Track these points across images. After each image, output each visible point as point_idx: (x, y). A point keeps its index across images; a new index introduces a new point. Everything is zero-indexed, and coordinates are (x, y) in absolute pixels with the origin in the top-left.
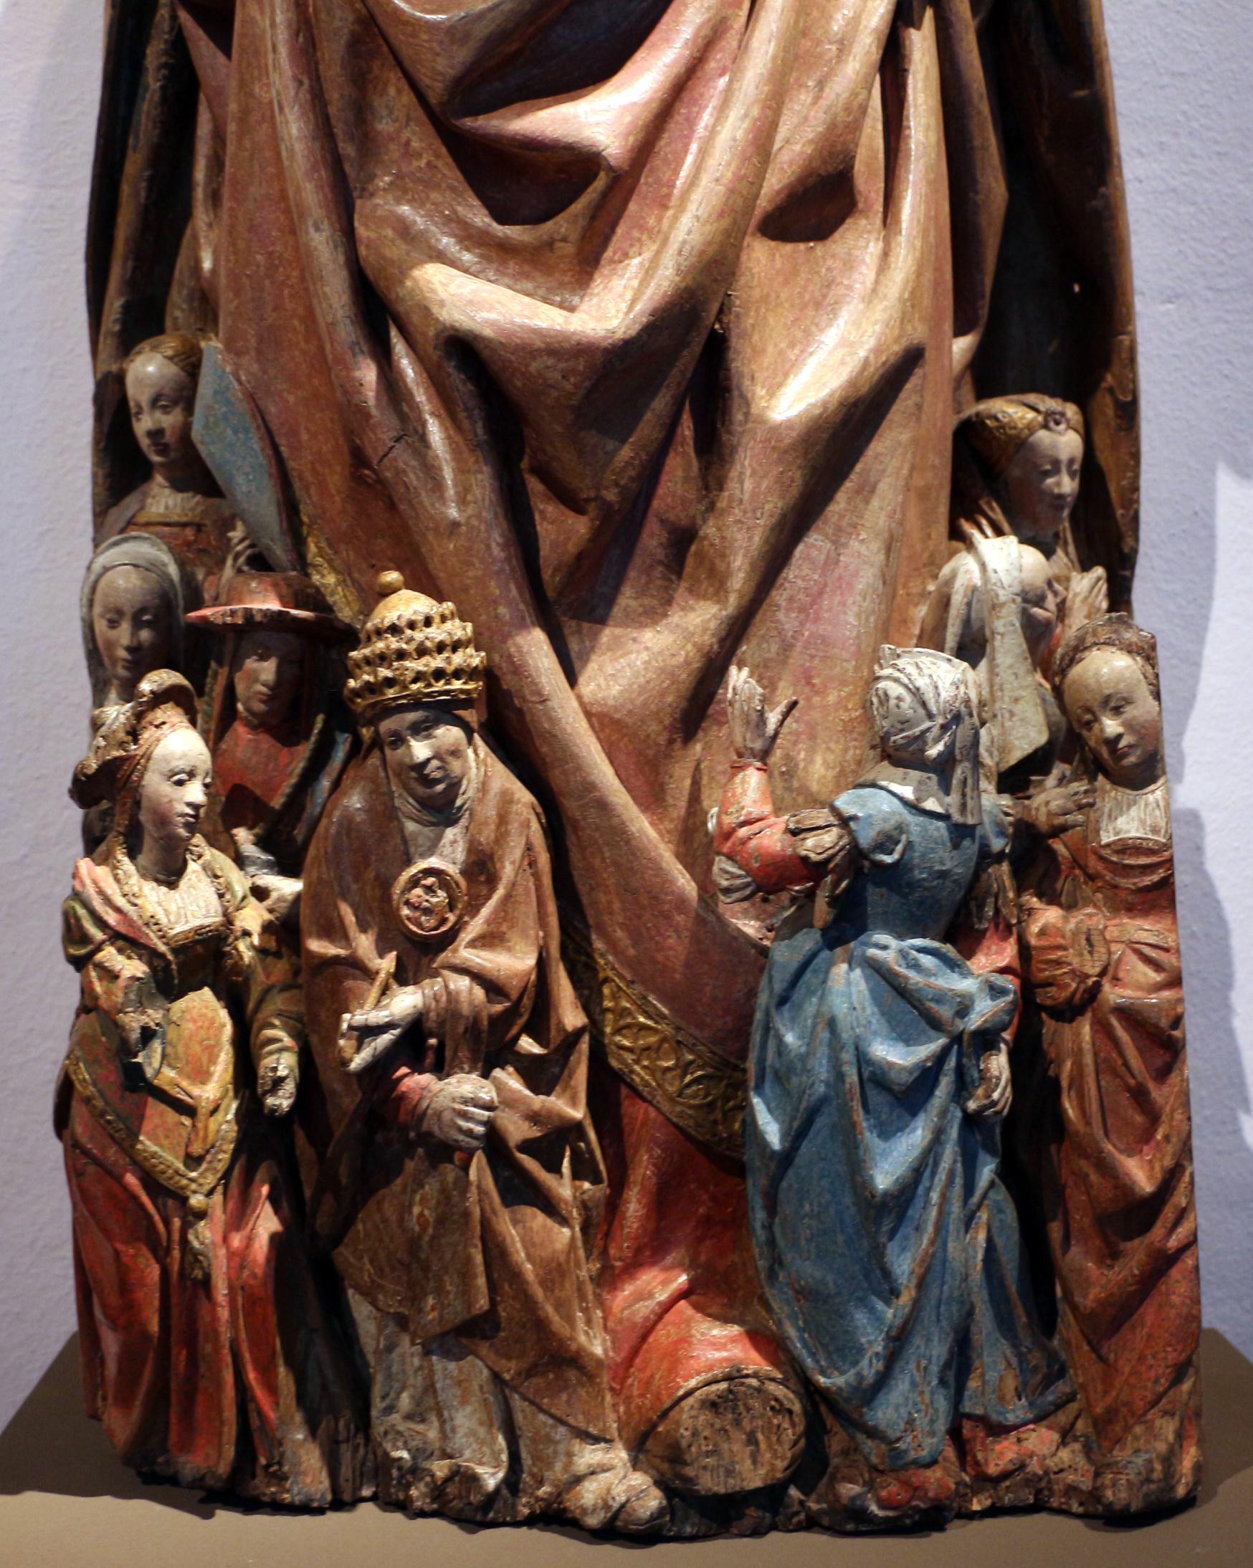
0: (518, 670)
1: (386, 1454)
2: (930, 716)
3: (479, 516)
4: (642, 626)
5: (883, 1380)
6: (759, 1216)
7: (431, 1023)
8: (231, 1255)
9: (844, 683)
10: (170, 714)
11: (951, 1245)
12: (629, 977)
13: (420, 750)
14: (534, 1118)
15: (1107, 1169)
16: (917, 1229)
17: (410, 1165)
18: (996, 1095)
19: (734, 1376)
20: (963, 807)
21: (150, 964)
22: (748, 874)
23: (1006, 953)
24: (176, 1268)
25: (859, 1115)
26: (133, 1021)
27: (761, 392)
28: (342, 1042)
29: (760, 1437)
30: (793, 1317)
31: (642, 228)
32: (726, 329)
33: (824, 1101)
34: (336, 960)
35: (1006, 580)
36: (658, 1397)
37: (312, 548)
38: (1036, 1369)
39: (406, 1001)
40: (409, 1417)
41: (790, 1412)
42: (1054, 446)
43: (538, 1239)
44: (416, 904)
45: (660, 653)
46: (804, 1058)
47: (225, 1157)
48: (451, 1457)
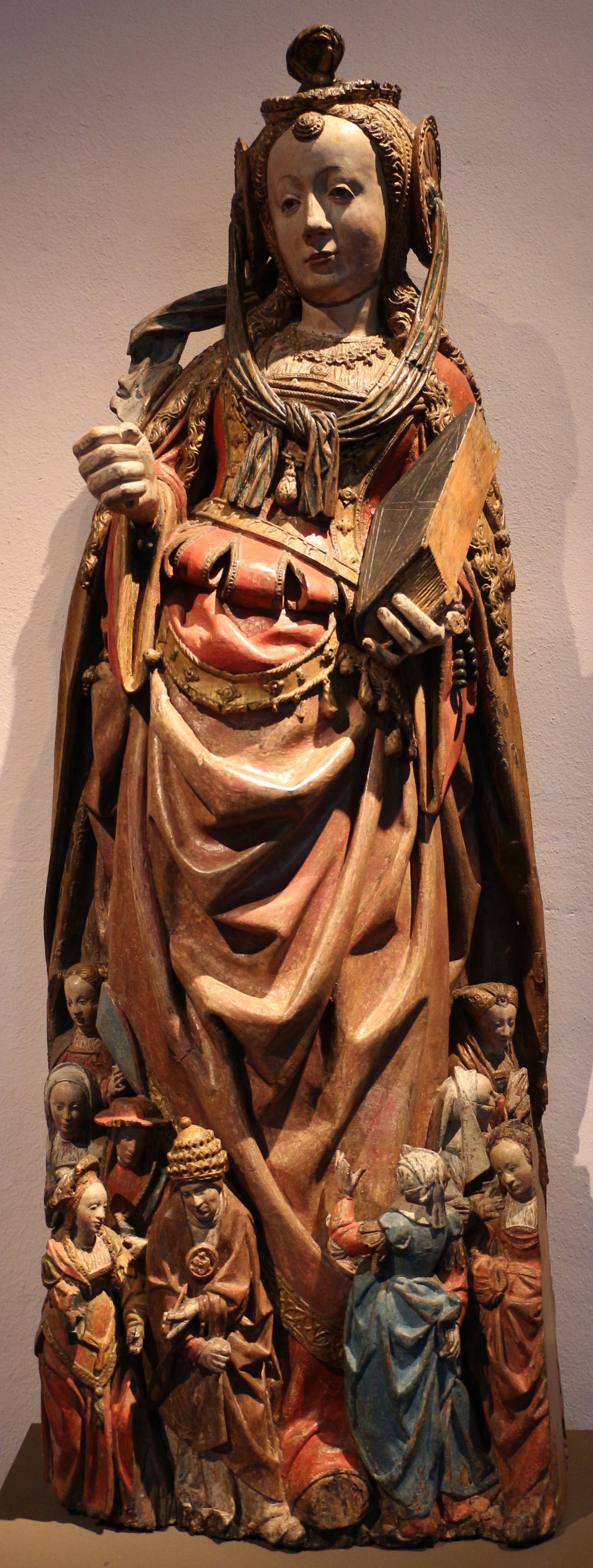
0: (242, 1156)
1: (181, 1504)
2: (421, 1184)
3: (224, 1088)
4: (298, 1130)
5: (402, 1478)
6: (350, 1397)
7: (202, 1317)
8: (113, 1414)
9: (390, 1152)
10: (91, 1177)
11: (433, 1416)
12: (291, 1289)
13: (198, 1200)
14: (248, 1355)
15: (506, 1380)
16: (418, 1409)
17: (193, 1375)
18: (452, 1350)
19: (336, 1473)
20: (437, 1221)
21: (80, 1288)
22: (342, 1249)
23: (459, 1281)
24: (89, 1419)
25: (392, 1362)
26: (73, 1314)
27: (350, 1028)
28: (163, 1326)
29: (348, 1502)
30: (364, 1446)
31: (297, 955)
32: (335, 999)
33: (374, 1352)
34: (161, 1286)
35: (469, 1095)
36: (302, 1482)
37: (151, 1083)
38: (478, 1469)
39: (192, 1307)
40: (192, 1486)
41: (361, 1491)
42: (501, 1013)
43: (248, 1409)
44: (197, 1263)
45: (306, 1143)
46: (367, 1331)
47: (111, 1370)
48: (210, 1507)
